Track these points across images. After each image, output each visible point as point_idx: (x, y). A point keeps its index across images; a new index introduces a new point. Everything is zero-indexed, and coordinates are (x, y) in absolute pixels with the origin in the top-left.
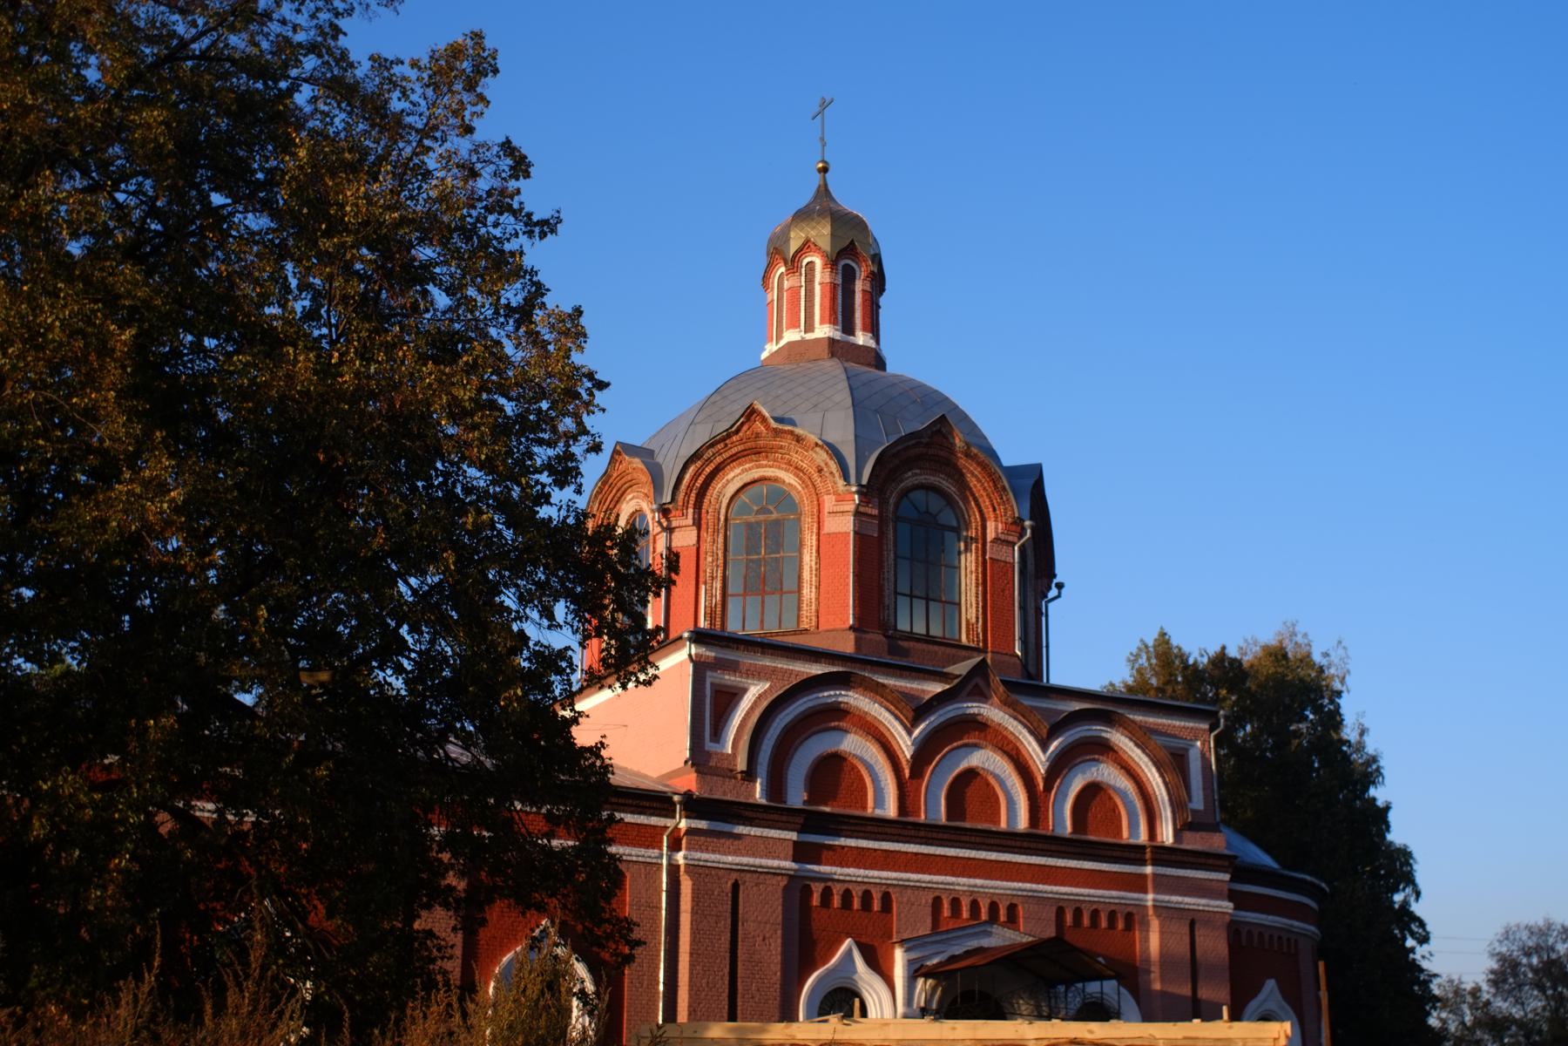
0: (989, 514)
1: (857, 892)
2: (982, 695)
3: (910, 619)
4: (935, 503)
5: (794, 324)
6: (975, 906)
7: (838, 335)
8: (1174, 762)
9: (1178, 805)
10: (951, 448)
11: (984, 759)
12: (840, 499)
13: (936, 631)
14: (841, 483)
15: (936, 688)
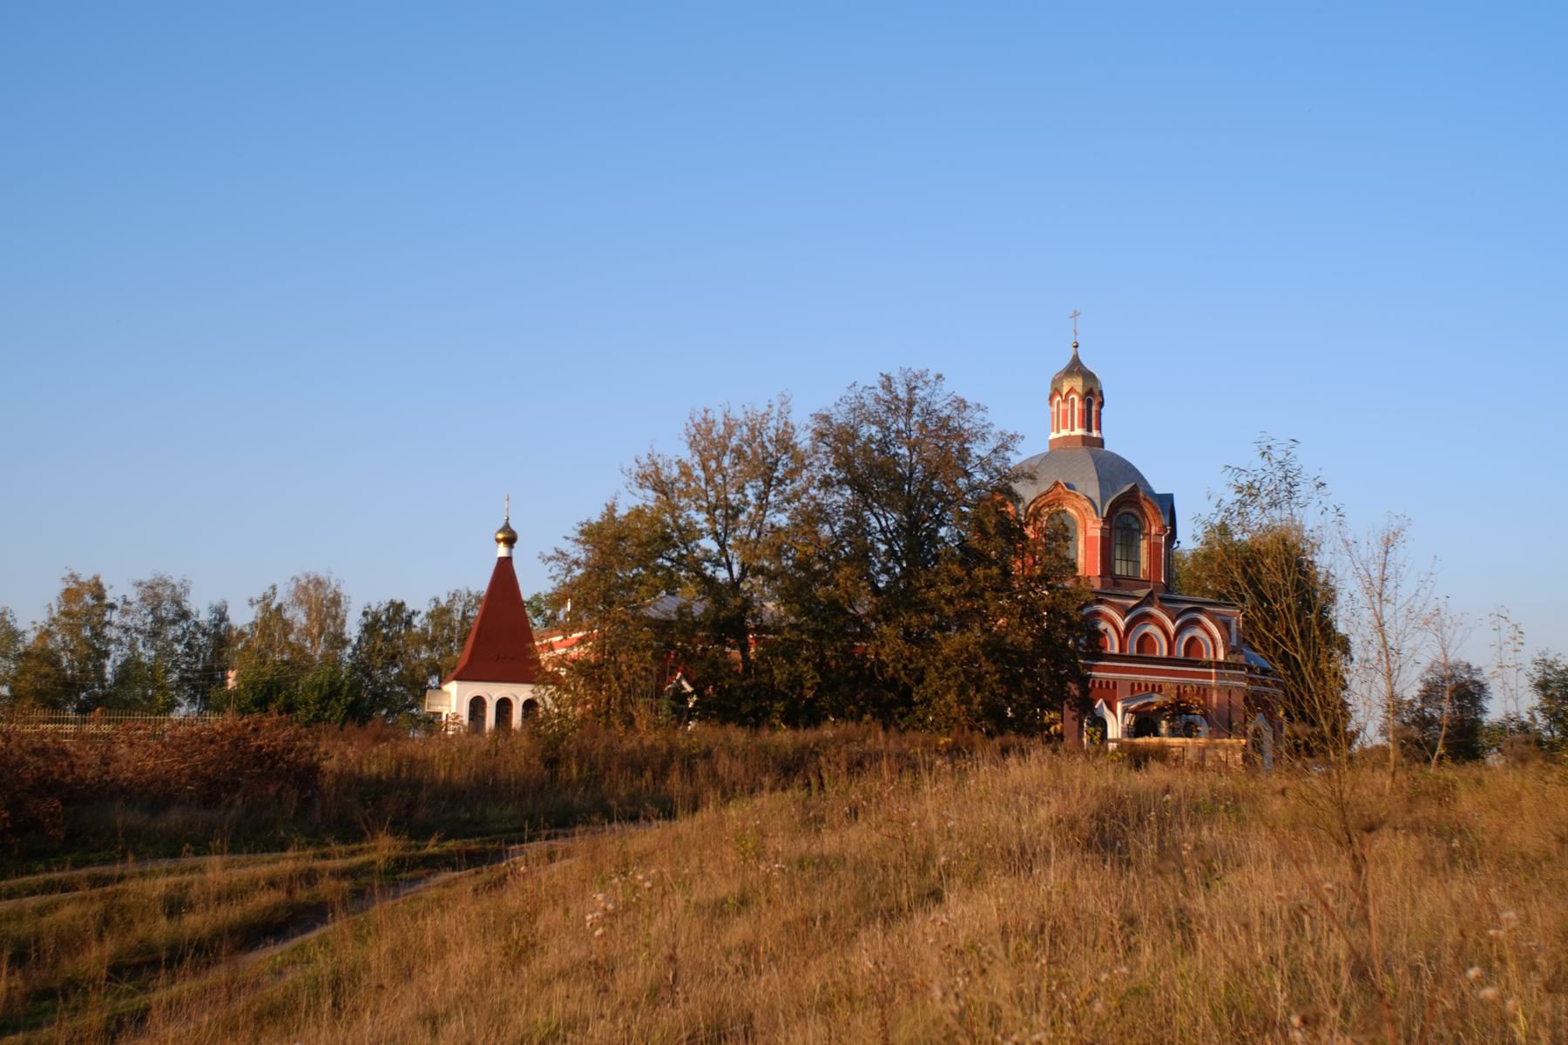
0: (1152, 523)
1: (1104, 682)
2: (1151, 605)
3: (1120, 568)
4: (1131, 519)
5: (1065, 426)
6: (1147, 686)
7: (1085, 433)
8: (1225, 626)
9: (1226, 647)
10: (1138, 497)
11: (1152, 629)
12: (1094, 522)
13: (1130, 574)
14: (1095, 516)
15: (1134, 602)
